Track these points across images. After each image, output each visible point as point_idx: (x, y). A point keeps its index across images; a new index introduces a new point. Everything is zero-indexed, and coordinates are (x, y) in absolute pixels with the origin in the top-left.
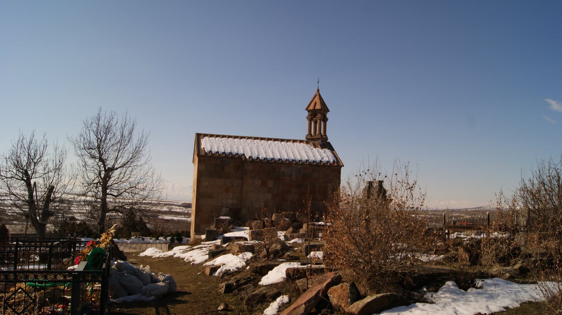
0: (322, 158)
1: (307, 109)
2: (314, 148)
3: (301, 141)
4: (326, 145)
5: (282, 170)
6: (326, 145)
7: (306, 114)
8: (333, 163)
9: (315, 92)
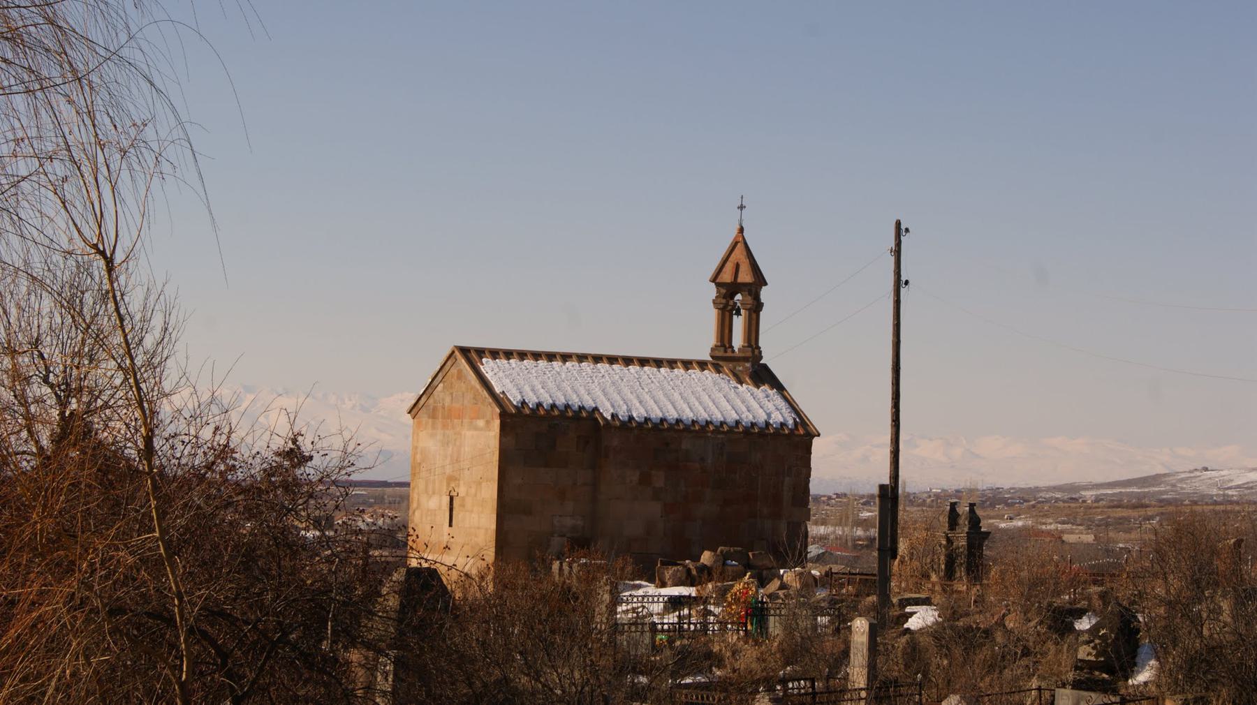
0: (769, 415)
1: (714, 280)
2: (739, 386)
3: (702, 365)
4: (763, 376)
5: (683, 447)
6: (763, 376)
7: (712, 291)
8: (793, 427)
9: (735, 232)
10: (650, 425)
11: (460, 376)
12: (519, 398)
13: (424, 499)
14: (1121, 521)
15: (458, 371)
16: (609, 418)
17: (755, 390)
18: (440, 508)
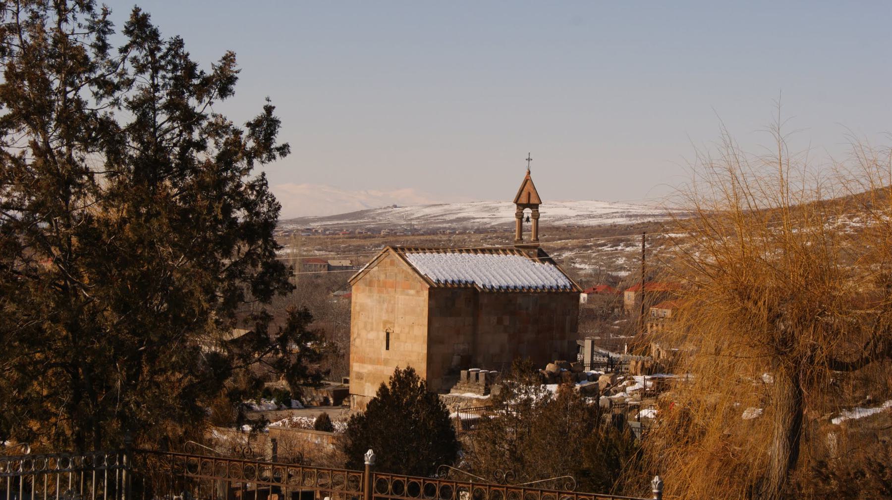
5: (518, 302)
9: (525, 174)
10: (503, 291)
11: (392, 263)
12: (435, 278)
13: (363, 333)
14: (358, 248)
15: (391, 260)
16: (482, 287)
17: (543, 265)
18: (378, 339)
